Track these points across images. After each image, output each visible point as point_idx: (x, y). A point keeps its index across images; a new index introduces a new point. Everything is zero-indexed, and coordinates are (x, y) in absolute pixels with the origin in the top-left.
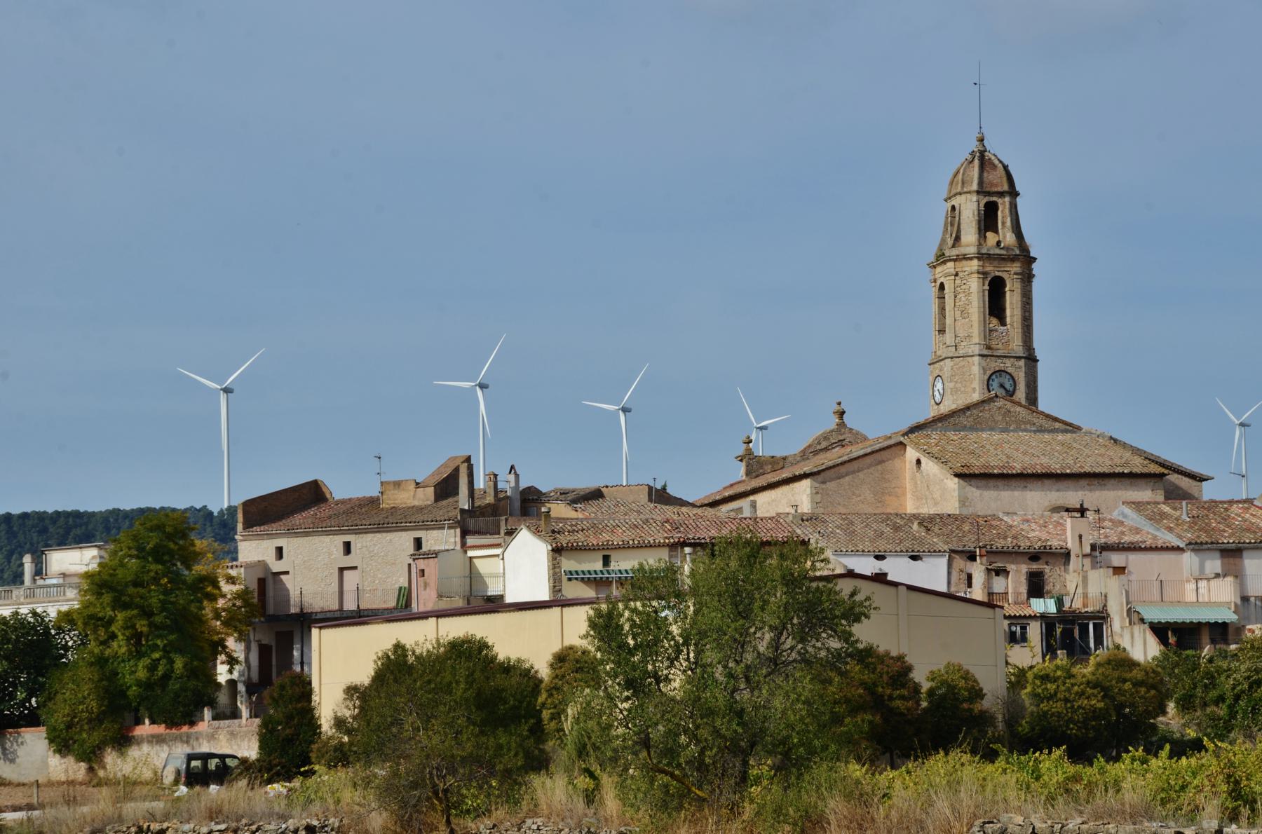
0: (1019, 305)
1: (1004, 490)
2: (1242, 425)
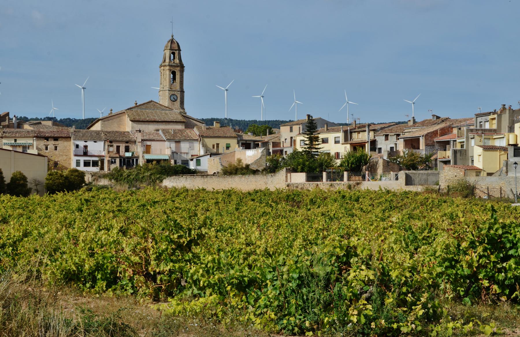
2: (102, 113)
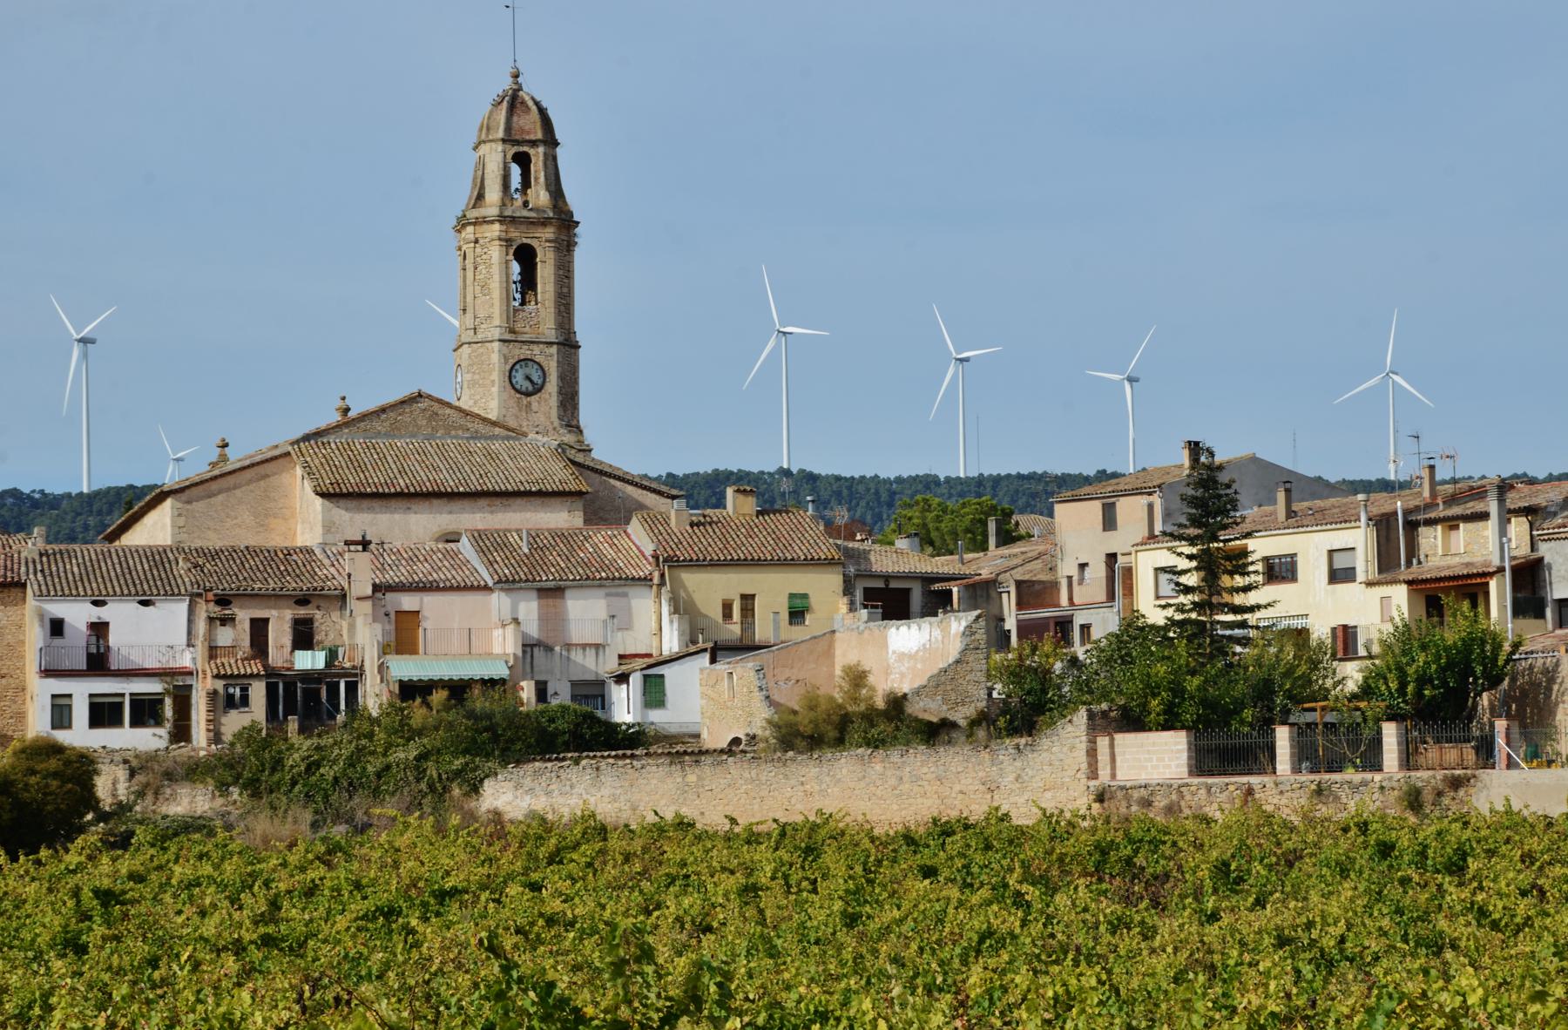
0: (552, 279)
1: (381, 513)
